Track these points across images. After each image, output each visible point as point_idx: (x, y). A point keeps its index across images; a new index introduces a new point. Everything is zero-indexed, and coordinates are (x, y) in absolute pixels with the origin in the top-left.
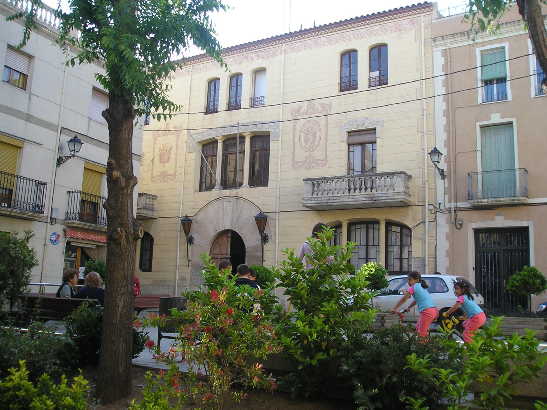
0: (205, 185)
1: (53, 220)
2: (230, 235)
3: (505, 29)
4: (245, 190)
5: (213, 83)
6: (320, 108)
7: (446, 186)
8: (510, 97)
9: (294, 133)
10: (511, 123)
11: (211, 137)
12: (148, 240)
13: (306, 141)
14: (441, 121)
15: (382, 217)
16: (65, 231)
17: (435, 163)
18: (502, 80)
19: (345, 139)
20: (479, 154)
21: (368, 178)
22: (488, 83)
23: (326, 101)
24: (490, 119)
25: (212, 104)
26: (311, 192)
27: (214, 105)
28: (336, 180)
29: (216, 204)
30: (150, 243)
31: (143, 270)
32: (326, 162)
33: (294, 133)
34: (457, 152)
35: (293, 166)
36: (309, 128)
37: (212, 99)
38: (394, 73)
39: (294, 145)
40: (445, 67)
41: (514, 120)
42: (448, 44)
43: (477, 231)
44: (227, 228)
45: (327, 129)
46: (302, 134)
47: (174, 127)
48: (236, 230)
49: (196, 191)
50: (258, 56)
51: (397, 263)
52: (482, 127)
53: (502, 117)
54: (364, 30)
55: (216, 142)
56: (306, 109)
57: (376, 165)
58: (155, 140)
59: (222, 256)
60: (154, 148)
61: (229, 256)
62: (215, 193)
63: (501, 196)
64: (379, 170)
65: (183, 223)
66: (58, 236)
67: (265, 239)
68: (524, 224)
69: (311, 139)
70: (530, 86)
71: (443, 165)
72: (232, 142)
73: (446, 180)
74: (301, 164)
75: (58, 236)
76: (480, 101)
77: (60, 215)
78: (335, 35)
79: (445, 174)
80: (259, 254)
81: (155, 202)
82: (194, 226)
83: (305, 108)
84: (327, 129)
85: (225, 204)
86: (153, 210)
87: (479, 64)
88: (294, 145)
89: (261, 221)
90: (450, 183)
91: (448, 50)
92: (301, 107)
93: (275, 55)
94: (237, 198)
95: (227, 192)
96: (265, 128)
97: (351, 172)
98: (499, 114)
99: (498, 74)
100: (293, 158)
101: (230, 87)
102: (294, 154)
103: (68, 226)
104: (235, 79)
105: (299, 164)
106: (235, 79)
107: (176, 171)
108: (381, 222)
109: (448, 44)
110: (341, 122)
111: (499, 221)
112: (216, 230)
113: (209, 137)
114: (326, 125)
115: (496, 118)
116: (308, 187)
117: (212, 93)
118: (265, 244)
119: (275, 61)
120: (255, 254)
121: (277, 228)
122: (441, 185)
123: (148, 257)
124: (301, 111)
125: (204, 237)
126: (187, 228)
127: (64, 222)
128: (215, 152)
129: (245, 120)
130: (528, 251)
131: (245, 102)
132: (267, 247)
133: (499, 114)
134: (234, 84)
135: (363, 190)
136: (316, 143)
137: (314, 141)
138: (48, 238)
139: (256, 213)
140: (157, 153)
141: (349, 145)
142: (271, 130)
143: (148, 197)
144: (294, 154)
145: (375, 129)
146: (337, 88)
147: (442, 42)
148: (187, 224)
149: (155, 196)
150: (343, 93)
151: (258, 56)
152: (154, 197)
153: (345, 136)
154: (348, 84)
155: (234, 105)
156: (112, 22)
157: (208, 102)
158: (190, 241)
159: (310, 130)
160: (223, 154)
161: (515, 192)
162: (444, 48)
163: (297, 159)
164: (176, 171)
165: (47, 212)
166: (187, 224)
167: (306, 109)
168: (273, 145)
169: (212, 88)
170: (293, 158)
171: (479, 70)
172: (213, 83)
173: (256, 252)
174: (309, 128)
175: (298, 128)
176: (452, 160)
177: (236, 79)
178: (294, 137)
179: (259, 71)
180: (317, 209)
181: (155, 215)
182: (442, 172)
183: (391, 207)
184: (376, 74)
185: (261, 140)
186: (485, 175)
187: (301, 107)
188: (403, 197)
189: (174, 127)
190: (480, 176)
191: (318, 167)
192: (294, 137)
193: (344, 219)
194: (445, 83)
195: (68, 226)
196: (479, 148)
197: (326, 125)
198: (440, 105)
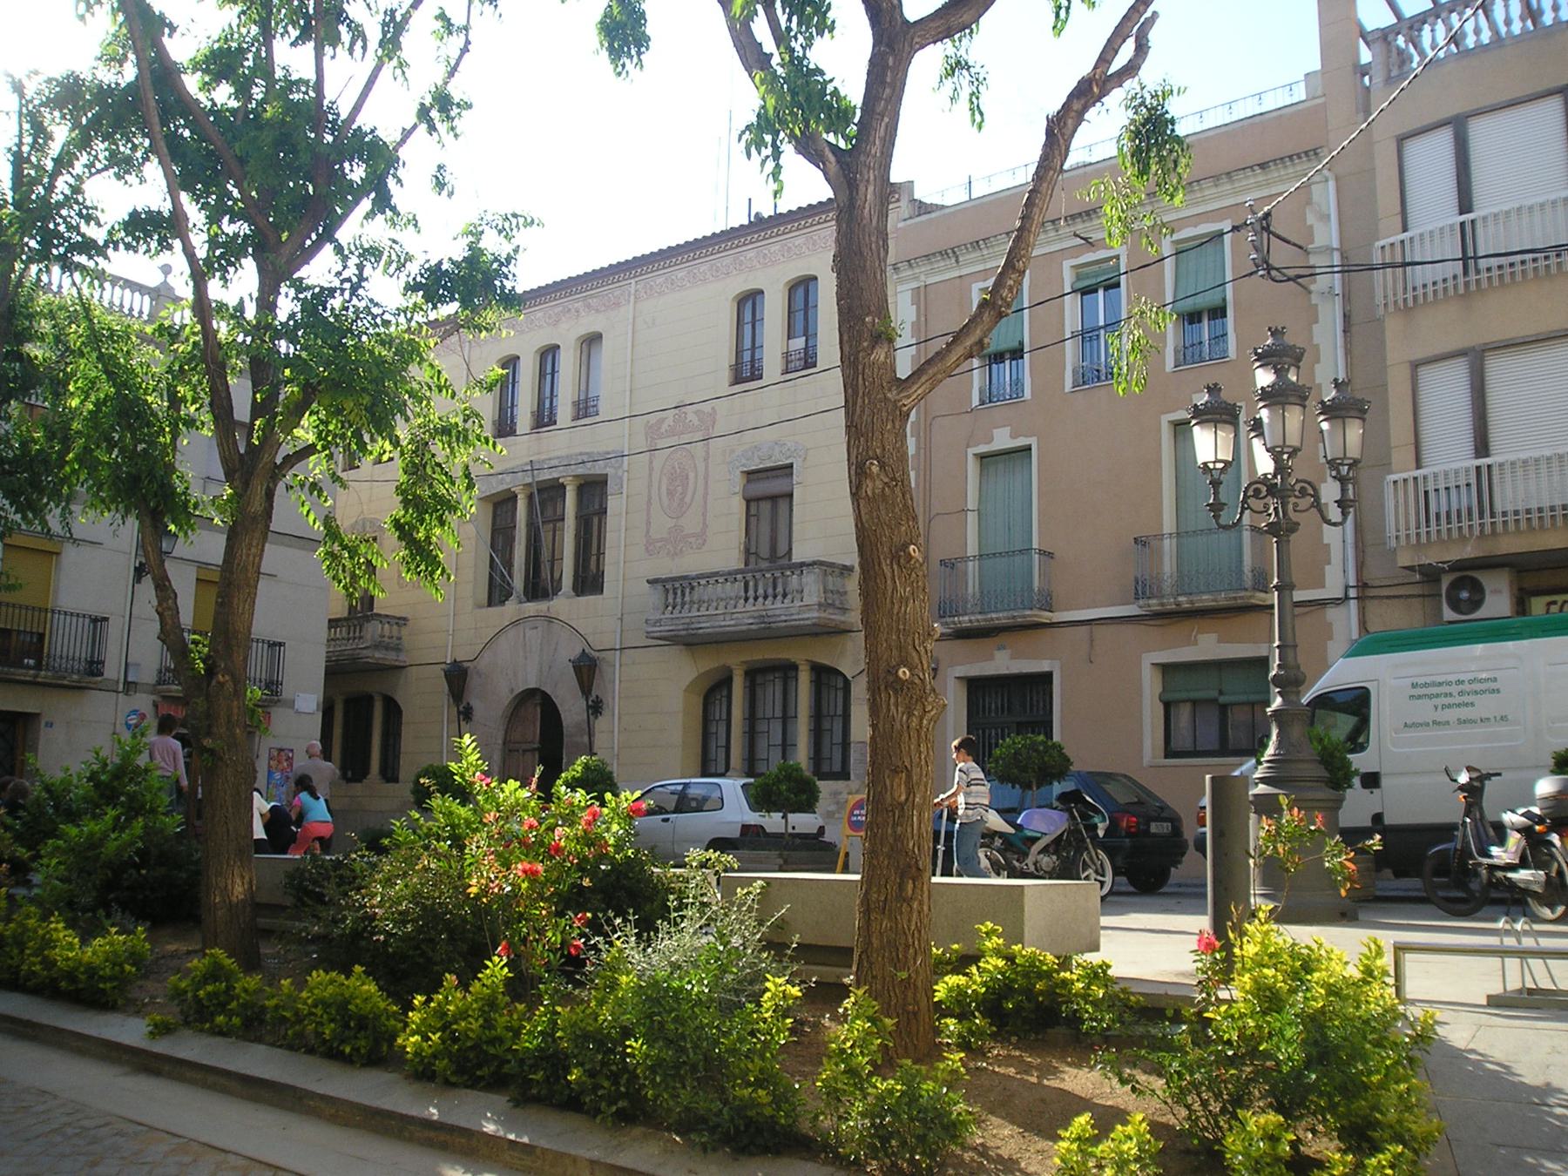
0: (497, 593)
1: (130, 687)
2: (538, 699)
4: (564, 605)
5: (750, 301)
8: (1028, 394)
10: (1029, 448)
11: (505, 487)
12: (393, 711)
13: (670, 493)
15: (798, 654)
16: (156, 705)
18: (1219, 312)
19: (738, 488)
20: (972, 519)
21: (758, 575)
22: (1193, 317)
23: (706, 407)
24: (991, 440)
25: (747, 356)
26: (662, 608)
27: (753, 360)
28: (703, 582)
29: (512, 633)
30: (840, 694)
31: (388, 781)
37: (747, 344)
39: (649, 502)
40: (916, 327)
41: (1033, 441)
42: (923, 277)
43: (1166, 669)
45: (707, 468)
46: (665, 481)
49: (480, 607)
50: (589, 306)
51: (837, 756)
52: (982, 457)
53: (1014, 436)
54: (751, 254)
55: (563, 487)
59: (524, 746)
62: (511, 609)
63: (1202, 588)
64: (797, 557)
65: (449, 675)
66: (143, 717)
67: (596, 708)
68: (1043, 666)
72: (549, 492)
75: (143, 717)
76: (976, 402)
77: (148, 675)
78: (725, 259)
80: (586, 739)
81: (405, 631)
82: (473, 682)
83: (670, 421)
84: (707, 468)
85: (529, 633)
86: (398, 649)
88: (649, 502)
89: (587, 669)
92: (663, 420)
93: (617, 305)
94: (550, 619)
95: (532, 608)
96: (598, 469)
97: (752, 559)
99: (1210, 299)
101: (553, 372)
103: (164, 697)
104: (800, 292)
106: (749, 305)
109: (923, 277)
110: (733, 451)
111: (1207, 646)
113: (501, 488)
114: (706, 459)
115: (1003, 439)
116: (654, 597)
117: (748, 329)
119: (611, 319)
121: (617, 683)
123: (838, 738)
127: (153, 689)
128: (559, 512)
129: (562, 449)
130: (1051, 722)
131: (564, 412)
132: (600, 724)
134: (799, 303)
135: (751, 600)
136: (687, 499)
137: (684, 493)
138: (121, 720)
141: (748, 501)
142: (609, 471)
144: (648, 523)
145: (791, 466)
146: (726, 375)
147: (910, 272)
148: (457, 677)
149: (405, 619)
150: (738, 388)
151: (589, 306)
152: (402, 621)
153: (738, 482)
154: (746, 371)
155: (544, 419)
157: (739, 352)
160: (578, 517)
162: (914, 285)
165: (112, 670)
166: (457, 677)
168: (614, 504)
169: (748, 317)
171: (1229, 277)
172: (750, 301)
175: (657, 464)
177: (549, 354)
178: (650, 486)
179: (592, 341)
180: (691, 642)
181: (404, 658)
183: (816, 634)
184: (799, 343)
185: (593, 489)
186: (988, 563)
187: (663, 420)
188: (816, 614)
190: (1168, 545)
192: (650, 486)
193: (736, 661)
195: (164, 697)
196: (972, 503)
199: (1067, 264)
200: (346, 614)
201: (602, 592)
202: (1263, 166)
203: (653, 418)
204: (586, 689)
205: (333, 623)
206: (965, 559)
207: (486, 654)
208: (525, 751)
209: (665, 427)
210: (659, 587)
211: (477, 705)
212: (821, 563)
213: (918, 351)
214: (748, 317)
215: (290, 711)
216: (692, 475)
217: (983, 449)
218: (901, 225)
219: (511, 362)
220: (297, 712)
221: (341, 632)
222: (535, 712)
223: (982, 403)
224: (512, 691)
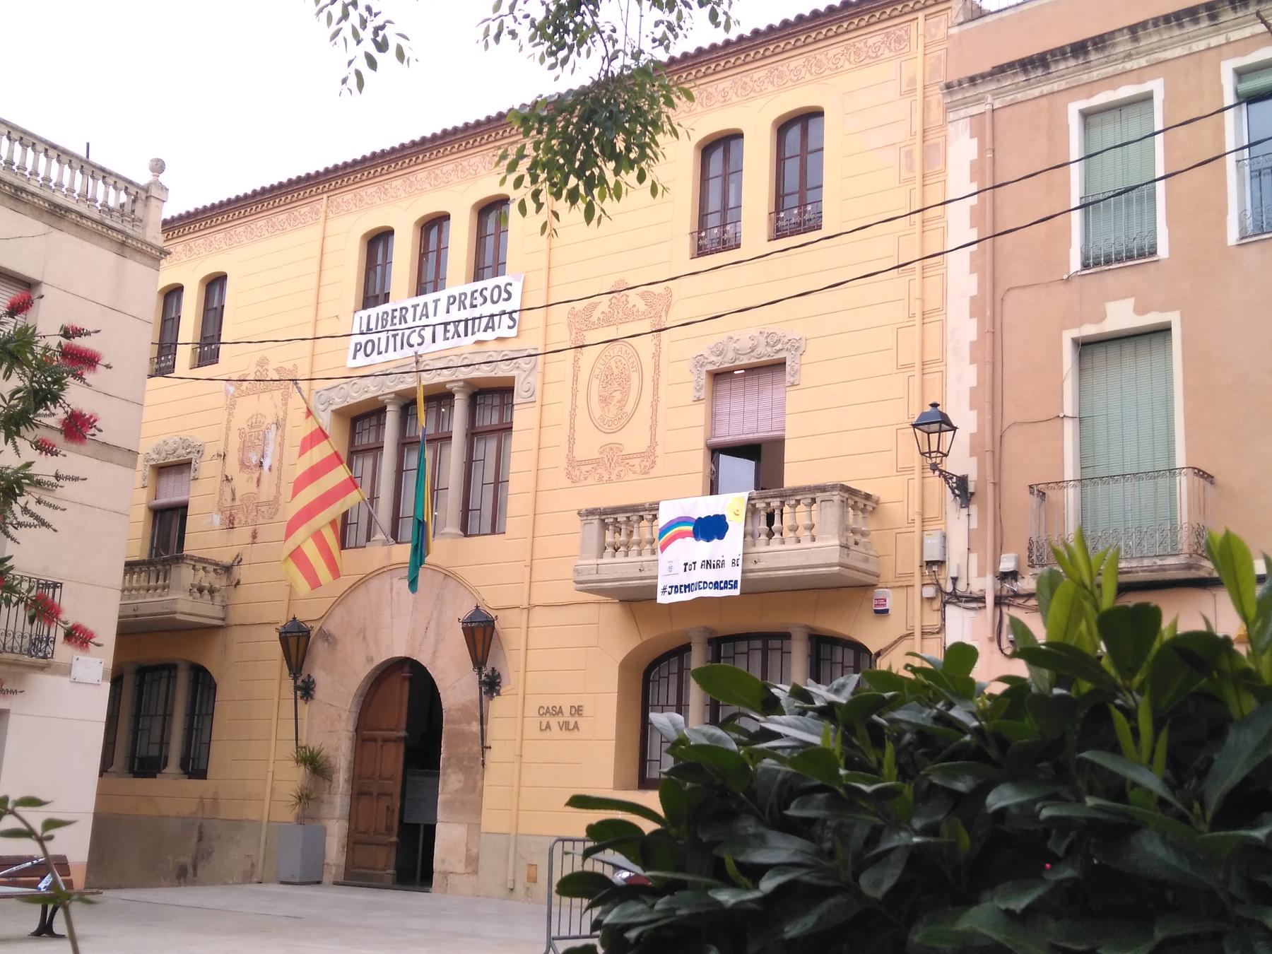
3: (1155, 39)
6: (641, 306)
7: (974, 525)
8: (1163, 251)
9: (575, 379)
12: (203, 685)
13: (605, 401)
14: (963, 329)
17: (934, 461)
20: (1069, 429)
24: (1102, 317)
32: (654, 462)
33: (575, 379)
34: (1006, 423)
35: (569, 475)
36: (613, 365)
38: (838, 198)
39: (573, 415)
40: (976, 169)
41: (1173, 318)
44: (400, 652)
47: (277, 370)
48: (424, 660)
52: (1085, 346)
53: (1140, 310)
56: (607, 310)
57: (943, 351)
58: (232, 406)
60: (228, 428)
61: (403, 734)
65: (284, 638)
67: (491, 685)
69: (618, 395)
70: (1224, 211)
71: (960, 462)
73: (974, 509)
74: (589, 468)
79: (971, 489)
80: (475, 727)
82: (319, 649)
87: (1075, 151)
88: (573, 415)
89: (481, 634)
90: (982, 519)
91: (988, 116)
92: (595, 306)
96: (502, 371)
98: (1129, 303)
100: (571, 450)
102: (572, 440)
105: (584, 468)
107: (278, 492)
108: (794, 635)
109: (990, 100)
112: (372, 660)
114: (657, 356)
115: (1121, 316)
117: (490, 242)
118: (492, 697)
120: (465, 727)
122: (959, 524)
124: (594, 318)
125: (341, 680)
126: (294, 661)
132: (497, 706)
133: (1129, 303)
136: (629, 408)
137: (622, 403)
139: (466, 610)
140: (235, 442)
143: (199, 566)
144: (572, 440)
146: (685, 244)
156: (1090, 801)
158: (306, 690)
159: (616, 371)
161: (1174, 543)
163: (580, 454)
164: (278, 492)
166: (297, 643)
167: (607, 310)
170: (571, 450)
172: (379, 241)
173: (469, 723)
174: (613, 365)
176: (993, 447)
182: (962, 490)
189: (277, 370)
190: (1071, 496)
191: (631, 476)
194: (976, 217)
196: (1069, 408)
197: (657, 356)
198: (961, 278)
199: (1227, 69)
200: (145, 557)
201: (723, 517)
202: (972, 80)
203: (579, 306)
204: (479, 661)
205: (130, 567)
206: (1060, 484)
207: (338, 613)
208: (385, 740)
209: (597, 314)
210: (595, 521)
211: (321, 677)
212: (845, 489)
213: (981, 202)
214: (433, 245)
215: (64, 681)
216: (635, 377)
217: (1090, 330)
218: (955, 30)
219: (173, 294)
220: (74, 681)
221: (139, 580)
222: (400, 692)
223: (1085, 266)
224: (370, 660)
